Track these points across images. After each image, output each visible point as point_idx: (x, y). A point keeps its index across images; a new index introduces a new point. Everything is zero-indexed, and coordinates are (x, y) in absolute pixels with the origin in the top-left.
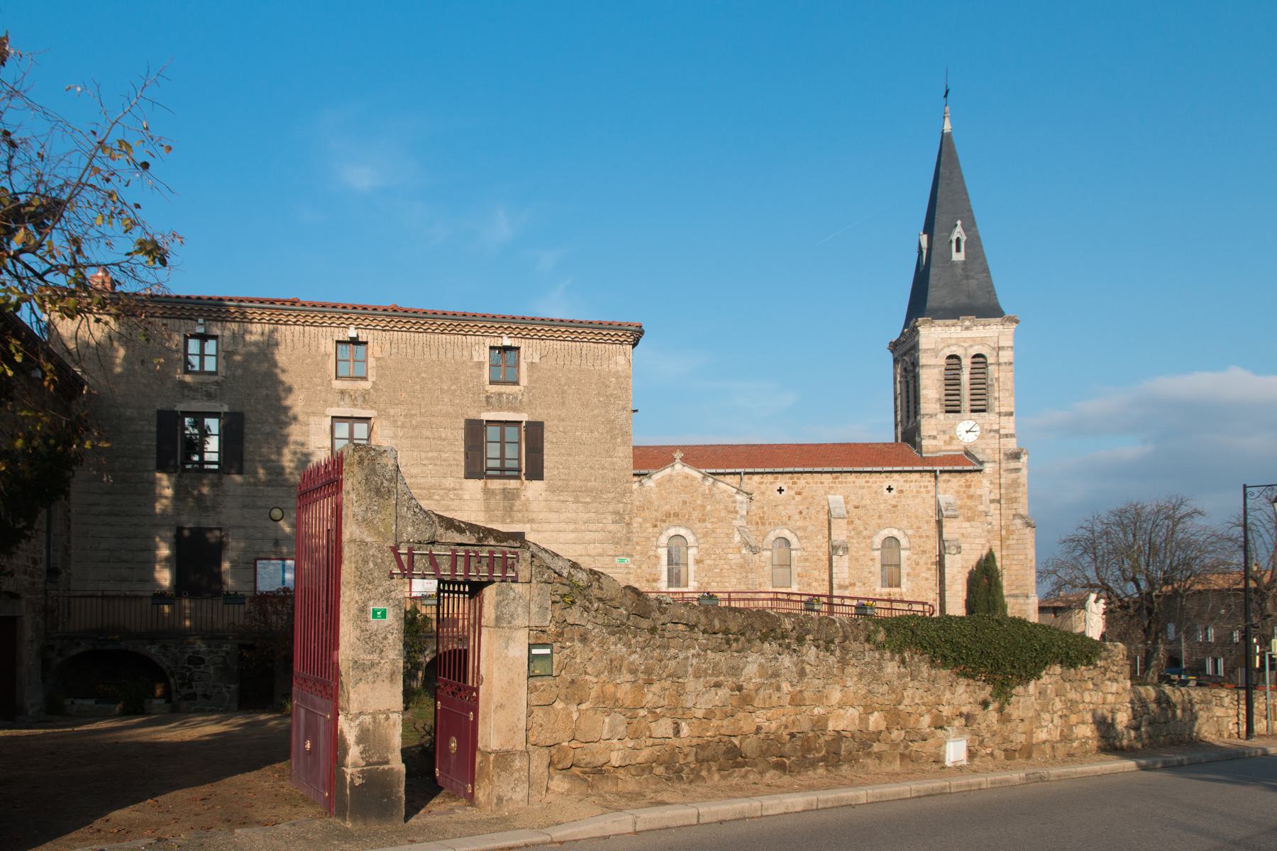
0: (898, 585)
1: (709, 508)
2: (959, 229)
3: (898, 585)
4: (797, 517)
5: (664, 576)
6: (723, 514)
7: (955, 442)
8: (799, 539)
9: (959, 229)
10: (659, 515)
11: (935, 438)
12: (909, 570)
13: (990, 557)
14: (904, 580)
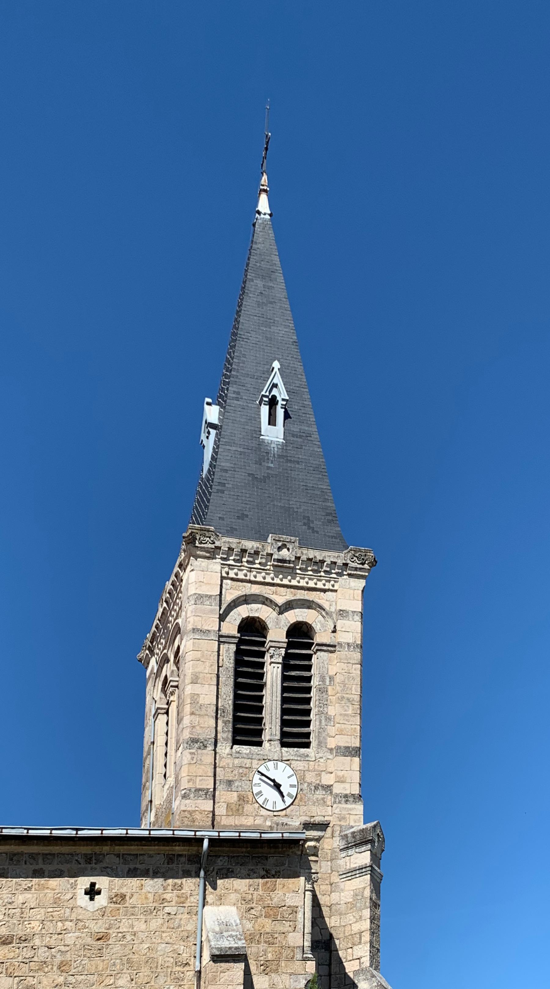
7: (248, 808)
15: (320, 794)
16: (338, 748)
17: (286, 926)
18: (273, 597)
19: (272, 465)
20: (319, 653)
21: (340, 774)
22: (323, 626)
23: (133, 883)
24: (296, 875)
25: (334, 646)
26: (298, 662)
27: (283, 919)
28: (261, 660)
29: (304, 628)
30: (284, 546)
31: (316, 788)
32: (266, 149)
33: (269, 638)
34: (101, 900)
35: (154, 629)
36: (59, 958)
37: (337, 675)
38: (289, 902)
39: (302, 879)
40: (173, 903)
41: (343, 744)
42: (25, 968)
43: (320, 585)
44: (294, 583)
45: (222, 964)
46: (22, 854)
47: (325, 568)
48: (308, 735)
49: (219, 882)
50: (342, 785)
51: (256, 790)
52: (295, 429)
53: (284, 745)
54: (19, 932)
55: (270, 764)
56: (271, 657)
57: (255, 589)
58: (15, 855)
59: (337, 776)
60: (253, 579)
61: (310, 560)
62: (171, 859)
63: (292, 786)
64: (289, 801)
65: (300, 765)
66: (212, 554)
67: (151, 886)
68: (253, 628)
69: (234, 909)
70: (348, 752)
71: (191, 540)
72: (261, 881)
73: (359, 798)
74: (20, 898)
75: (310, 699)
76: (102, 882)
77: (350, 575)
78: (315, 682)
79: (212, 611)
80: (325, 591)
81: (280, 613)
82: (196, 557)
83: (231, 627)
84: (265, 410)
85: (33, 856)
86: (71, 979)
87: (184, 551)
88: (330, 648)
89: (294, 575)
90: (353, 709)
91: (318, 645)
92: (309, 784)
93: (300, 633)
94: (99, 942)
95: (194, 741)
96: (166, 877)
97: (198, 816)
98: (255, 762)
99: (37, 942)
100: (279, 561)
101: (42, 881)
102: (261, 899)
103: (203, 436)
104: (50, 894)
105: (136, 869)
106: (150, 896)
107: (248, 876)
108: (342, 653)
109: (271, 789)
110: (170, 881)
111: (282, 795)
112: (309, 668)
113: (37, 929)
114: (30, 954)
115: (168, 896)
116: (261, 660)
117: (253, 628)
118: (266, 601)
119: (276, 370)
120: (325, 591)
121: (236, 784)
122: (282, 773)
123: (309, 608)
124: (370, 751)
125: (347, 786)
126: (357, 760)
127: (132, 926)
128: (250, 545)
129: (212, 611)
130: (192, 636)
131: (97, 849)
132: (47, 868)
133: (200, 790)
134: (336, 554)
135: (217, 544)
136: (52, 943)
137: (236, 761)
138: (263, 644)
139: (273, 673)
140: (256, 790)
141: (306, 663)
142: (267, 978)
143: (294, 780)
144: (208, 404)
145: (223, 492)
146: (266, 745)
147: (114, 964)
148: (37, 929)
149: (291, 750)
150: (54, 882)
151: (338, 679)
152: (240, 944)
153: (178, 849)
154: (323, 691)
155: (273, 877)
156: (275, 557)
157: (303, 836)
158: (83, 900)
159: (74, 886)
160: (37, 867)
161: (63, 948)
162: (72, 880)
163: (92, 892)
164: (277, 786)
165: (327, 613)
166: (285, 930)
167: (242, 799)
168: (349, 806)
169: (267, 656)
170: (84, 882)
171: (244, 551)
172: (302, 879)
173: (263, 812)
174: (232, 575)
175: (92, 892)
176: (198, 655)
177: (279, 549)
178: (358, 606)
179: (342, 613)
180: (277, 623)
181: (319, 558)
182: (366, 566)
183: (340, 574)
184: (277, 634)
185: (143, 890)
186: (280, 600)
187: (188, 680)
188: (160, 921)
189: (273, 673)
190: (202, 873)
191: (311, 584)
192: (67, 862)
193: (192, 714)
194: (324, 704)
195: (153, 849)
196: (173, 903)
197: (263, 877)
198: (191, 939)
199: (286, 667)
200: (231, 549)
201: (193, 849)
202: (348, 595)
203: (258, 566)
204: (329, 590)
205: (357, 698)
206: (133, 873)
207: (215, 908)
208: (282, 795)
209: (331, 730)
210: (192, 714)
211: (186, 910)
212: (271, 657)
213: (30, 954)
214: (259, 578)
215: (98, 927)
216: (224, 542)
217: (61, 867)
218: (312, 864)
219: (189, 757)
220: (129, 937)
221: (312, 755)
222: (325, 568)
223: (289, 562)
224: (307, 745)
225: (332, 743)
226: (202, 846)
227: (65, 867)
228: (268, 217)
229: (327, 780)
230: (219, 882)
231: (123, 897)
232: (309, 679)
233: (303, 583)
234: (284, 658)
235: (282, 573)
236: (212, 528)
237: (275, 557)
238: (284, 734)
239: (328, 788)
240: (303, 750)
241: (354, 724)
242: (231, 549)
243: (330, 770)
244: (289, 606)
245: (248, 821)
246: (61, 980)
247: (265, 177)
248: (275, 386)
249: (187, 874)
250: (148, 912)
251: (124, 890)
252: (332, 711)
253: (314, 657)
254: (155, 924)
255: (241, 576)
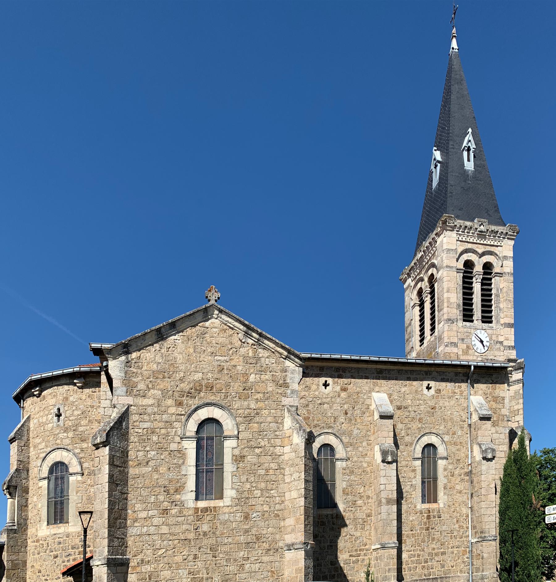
0: (435, 501)
1: (252, 378)
2: (469, 137)
3: (435, 501)
4: (342, 419)
5: (191, 484)
6: (271, 387)
7: (471, 352)
8: (345, 446)
9: (469, 137)
10: (185, 386)
11: (455, 345)
12: (445, 481)
13: (64, 574)
14: (441, 494)
15: (498, 345)
16: (505, 324)
17: (500, 406)
18: (477, 250)
19: (470, 182)
20: (496, 278)
21: (507, 336)
22: (497, 264)
23: (444, 384)
24: (504, 383)
25: (502, 274)
26: (486, 282)
27: (500, 402)
28: (471, 281)
29: (488, 265)
30: (482, 224)
31: (497, 343)
32: (455, 14)
33: (475, 271)
34: (432, 391)
35: (412, 264)
36: (418, 417)
37: (503, 287)
38: (501, 395)
39: (506, 384)
40: (458, 394)
41: (507, 322)
42: (407, 420)
43: (495, 244)
44: (485, 242)
45: (483, 421)
46: (402, 370)
47: (498, 235)
48: (491, 317)
49: (475, 385)
50: (508, 341)
51: (473, 343)
52: (478, 163)
53: (483, 322)
54: (404, 404)
55: (478, 331)
56: (476, 279)
57: (470, 246)
58: (400, 370)
59: (505, 337)
60: (469, 241)
61: (492, 231)
62: (457, 374)
63: (487, 342)
64: (486, 348)
65: (490, 332)
66: (453, 228)
67: (449, 386)
68: (469, 265)
69: (481, 397)
70: (509, 325)
71: (445, 222)
72: (490, 385)
73: (514, 348)
74: (403, 390)
75: (492, 300)
76: (432, 383)
77: (508, 238)
78: (493, 292)
79: (454, 257)
80: (497, 246)
81: (480, 257)
82: (447, 230)
83: (460, 265)
84: (465, 153)
85: (406, 371)
86: (423, 426)
87: (441, 227)
88: (500, 275)
89: (485, 239)
90: (511, 305)
91: (495, 273)
92: (494, 341)
93: (488, 267)
94: (433, 410)
95: (449, 320)
96: (455, 383)
97: (452, 355)
98: (472, 330)
99: (410, 409)
100: (480, 231)
101: (410, 382)
102: (491, 393)
103: (432, 167)
104: (414, 388)
105: (444, 378)
106: (450, 390)
107: (485, 383)
108: (506, 277)
109: (490, 341)
110: (457, 384)
111: (484, 346)
112: (490, 284)
113: (410, 403)
114: (408, 414)
115: (456, 391)
116: (471, 281)
117: (469, 265)
118: (474, 252)
119: (470, 133)
120: (497, 246)
121: (466, 340)
122: (483, 336)
123: (491, 255)
124: (518, 326)
125: (509, 342)
126: (513, 329)
127: (444, 404)
128: (468, 224)
129: (454, 257)
130: (446, 269)
131: (430, 369)
132: (412, 377)
133: (452, 343)
134: (503, 228)
135: (455, 223)
136: (416, 410)
137: (465, 330)
138: (472, 273)
139: (477, 287)
140: (473, 343)
141: (489, 282)
142: (494, 428)
143: (488, 339)
144: (435, 150)
145: (452, 197)
146: (475, 322)
147: (438, 420)
148: (410, 403)
149: (485, 324)
150: (415, 383)
151: (505, 290)
152: (490, 413)
153: (459, 370)
154: (497, 296)
155: (495, 383)
156: (478, 230)
157: (506, 365)
158: (425, 391)
159: (422, 385)
160: (408, 376)
161: (420, 412)
162: (421, 382)
163: (428, 388)
164: (482, 342)
165: (499, 258)
166: (500, 407)
167: (468, 347)
168: (510, 351)
169: (474, 279)
170: (425, 383)
171: (466, 227)
172: (506, 384)
173: (476, 354)
174: (460, 239)
175: (428, 388)
176: (449, 278)
177: (480, 225)
178: (511, 254)
179: (505, 258)
180: (479, 263)
181: (496, 230)
182: (515, 234)
183: (504, 238)
184: (478, 268)
185: (447, 387)
186: (480, 251)
187: (445, 290)
188: (454, 402)
189: (477, 287)
190: (469, 381)
191: (492, 243)
192: (419, 374)
193: (448, 307)
194: (498, 302)
195: (450, 369)
196: (458, 394)
197: (491, 384)
198: (466, 410)
199: (482, 284)
200: (461, 226)
201: (465, 370)
202: (506, 248)
203: (471, 234)
204: (499, 246)
205: (512, 299)
206: (443, 380)
207: (474, 397)
208: (484, 346)
209: (502, 315)
210: (448, 307)
211: (463, 397)
212: (476, 279)
213: (408, 414)
214: (471, 241)
215: (432, 403)
216: (458, 222)
217: (416, 376)
218: (510, 378)
219: (447, 327)
220: (443, 409)
221: (494, 327)
222: (498, 235)
223: (484, 232)
224: (491, 322)
225: (502, 321)
226: (471, 369)
227: (418, 376)
228: (457, 50)
229: (501, 339)
230: (475, 385)
231: (440, 390)
232: (491, 290)
233: (489, 243)
234: (482, 280)
235: (480, 237)
236: (453, 216)
237: (478, 230)
238: (483, 317)
239: (501, 343)
240: (490, 325)
241: (512, 312)
242: (461, 226)
243: (502, 334)
244: (483, 254)
245: (471, 358)
246: (420, 426)
247: (455, 29)
248: (470, 141)
249: (463, 381)
250: (450, 398)
251: (440, 388)
252: (501, 306)
253: (493, 280)
254: (452, 402)
255: (464, 240)
